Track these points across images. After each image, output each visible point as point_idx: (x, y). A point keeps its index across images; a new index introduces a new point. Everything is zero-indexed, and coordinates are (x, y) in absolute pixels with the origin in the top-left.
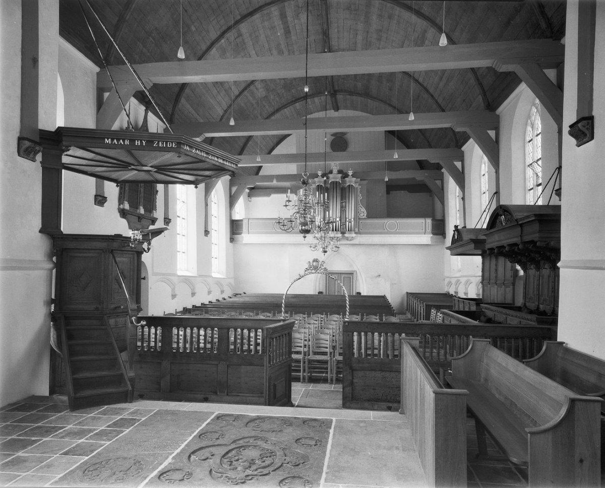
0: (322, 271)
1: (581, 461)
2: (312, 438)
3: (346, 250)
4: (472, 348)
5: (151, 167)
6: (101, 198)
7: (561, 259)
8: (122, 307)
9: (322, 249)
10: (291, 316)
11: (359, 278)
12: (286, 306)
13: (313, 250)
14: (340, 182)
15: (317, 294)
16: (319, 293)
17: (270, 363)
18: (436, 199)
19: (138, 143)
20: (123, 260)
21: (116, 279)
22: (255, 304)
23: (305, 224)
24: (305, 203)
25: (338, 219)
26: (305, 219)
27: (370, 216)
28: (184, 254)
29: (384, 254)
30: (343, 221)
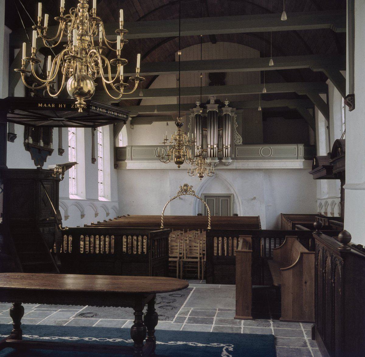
0: (190, 193)
1: (306, 283)
2: (180, 294)
3: (227, 176)
4: (285, 243)
5: (64, 118)
6: (12, 135)
7: (346, 183)
8: (48, 220)
9: (198, 175)
10: (81, 25)
11: (236, 201)
12: (164, 224)
13: (191, 175)
14: (217, 111)
15: (197, 215)
16: (198, 215)
17: (153, 257)
18: (311, 129)
19: (60, 106)
20: (47, 185)
21: (42, 200)
22: (138, 223)
23: (179, 157)
24: (179, 141)
25: (215, 146)
26: (179, 154)
27: (245, 143)
28: (101, 184)
29: (259, 178)
30: (220, 147)
